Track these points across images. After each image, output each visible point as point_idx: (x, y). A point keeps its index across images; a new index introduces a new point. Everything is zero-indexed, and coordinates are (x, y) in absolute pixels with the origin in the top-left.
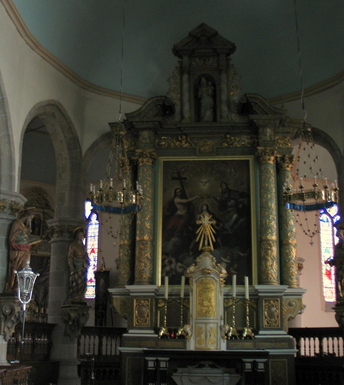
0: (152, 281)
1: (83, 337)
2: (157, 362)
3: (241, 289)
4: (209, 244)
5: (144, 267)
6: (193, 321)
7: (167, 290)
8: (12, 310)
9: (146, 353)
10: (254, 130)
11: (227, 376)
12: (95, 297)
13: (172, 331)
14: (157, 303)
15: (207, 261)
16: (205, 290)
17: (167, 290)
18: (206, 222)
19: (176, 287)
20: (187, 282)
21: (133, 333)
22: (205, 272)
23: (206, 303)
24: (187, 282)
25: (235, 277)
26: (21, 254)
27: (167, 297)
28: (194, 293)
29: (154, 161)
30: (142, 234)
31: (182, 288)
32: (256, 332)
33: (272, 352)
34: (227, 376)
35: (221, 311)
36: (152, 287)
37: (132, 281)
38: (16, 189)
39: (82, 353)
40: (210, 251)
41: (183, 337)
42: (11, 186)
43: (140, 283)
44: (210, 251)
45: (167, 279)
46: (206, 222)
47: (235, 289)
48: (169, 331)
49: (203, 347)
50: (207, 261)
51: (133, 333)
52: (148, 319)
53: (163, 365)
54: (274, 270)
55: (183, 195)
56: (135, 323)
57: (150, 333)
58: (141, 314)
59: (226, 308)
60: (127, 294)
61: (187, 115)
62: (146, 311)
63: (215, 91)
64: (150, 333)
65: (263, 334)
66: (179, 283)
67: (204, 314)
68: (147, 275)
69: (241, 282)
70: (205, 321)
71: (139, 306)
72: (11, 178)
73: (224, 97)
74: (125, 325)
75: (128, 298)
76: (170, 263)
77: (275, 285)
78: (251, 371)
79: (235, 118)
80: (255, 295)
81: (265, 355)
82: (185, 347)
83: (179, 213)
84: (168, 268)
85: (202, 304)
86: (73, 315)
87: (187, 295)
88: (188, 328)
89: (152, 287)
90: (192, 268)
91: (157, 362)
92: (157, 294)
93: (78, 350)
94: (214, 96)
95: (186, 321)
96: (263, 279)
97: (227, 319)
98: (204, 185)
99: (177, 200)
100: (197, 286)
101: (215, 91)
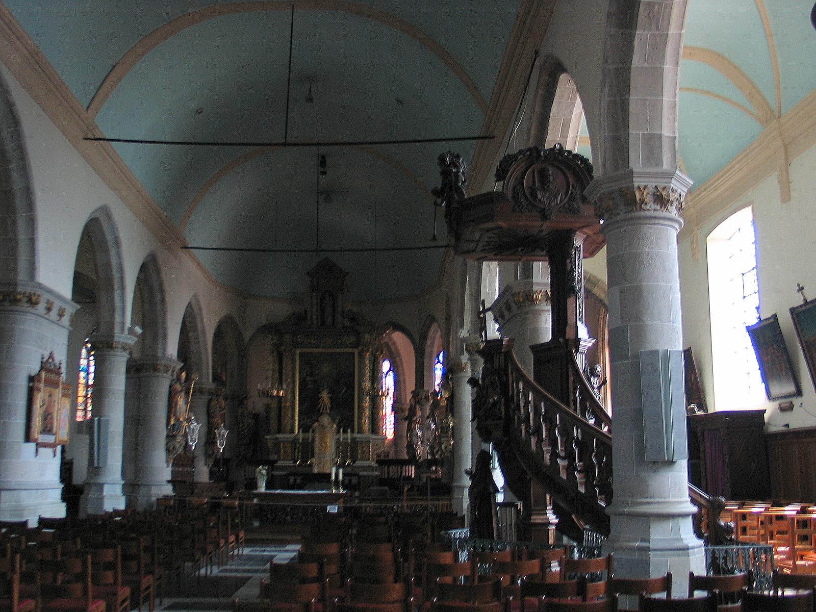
0: (292, 431)
1: (247, 466)
2: (295, 480)
3: (345, 436)
4: (326, 409)
5: (287, 421)
6: (316, 456)
7: (301, 436)
8: (213, 452)
9: (289, 475)
10: (358, 335)
11: (211, 569)
12: (470, 503)
13: (304, 461)
14: (295, 444)
15: (326, 420)
16: (323, 438)
17: (301, 436)
18: (325, 395)
19: (307, 435)
20: (313, 432)
21: (280, 463)
22: (323, 427)
23: (324, 445)
24: (313, 432)
25: (342, 429)
26: (217, 419)
27: (301, 441)
28: (317, 438)
29: (293, 354)
30: (286, 403)
31: (310, 434)
32: (354, 462)
33: (362, 473)
34: (211, 569)
35: (333, 450)
36: (292, 436)
37: (279, 432)
38: (211, 380)
39: (247, 477)
40: (327, 413)
41: (311, 465)
42: (208, 379)
43: (284, 433)
44: (327, 413)
45: (301, 430)
46: (325, 395)
47: (342, 436)
48: (302, 462)
49: (322, 471)
50: (326, 420)
51: (280, 463)
52: (290, 455)
53: (298, 481)
54: (366, 424)
55: (312, 375)
56: (282, 457)
57: (290, 463)
58: (285, 452)
59: (337, 448)
60: (277, 439)
61: (315, 322)
62: (289, 449)
63: (334, 304)
64: (290, 463)
65: (358, 463)
66: (308, 431)
67: (323, 451)
68: (289, 427)
69: (345, 432)
70: (440, 506)
71: (285, 447)
72: (208, 373)
73: (340, 309)
74: (275, 457)
75: (277, 443)
76: (304, 419)
77: (367, 434)
78: (520, 264)
79: (347, 323)
80: (353, 439)
81: (355, 475)
82: (312, 470)
83: (309, 386)
84: (301, 423)
85: (321, 446)
86: (243, 453)
87: (313, 439)
88: (313, 460)
89: (292, 436)
90: (316, 424)
91: (295, 480)
92: (295, 440)
93: (245, 475)
94: (334, 307)
95: (313, 456)
96: (360, 431)
97: (337, 455)
98: (326, 369)
99: (308, 378)
100: (319, 435)
101: (334, 304)
